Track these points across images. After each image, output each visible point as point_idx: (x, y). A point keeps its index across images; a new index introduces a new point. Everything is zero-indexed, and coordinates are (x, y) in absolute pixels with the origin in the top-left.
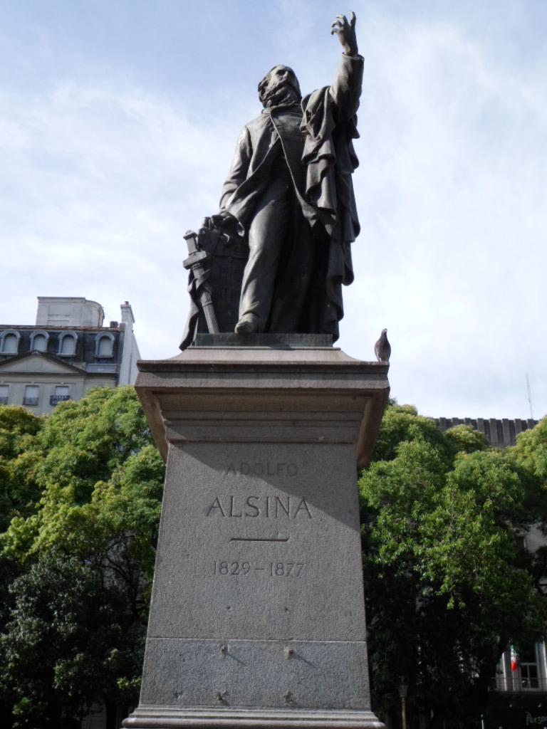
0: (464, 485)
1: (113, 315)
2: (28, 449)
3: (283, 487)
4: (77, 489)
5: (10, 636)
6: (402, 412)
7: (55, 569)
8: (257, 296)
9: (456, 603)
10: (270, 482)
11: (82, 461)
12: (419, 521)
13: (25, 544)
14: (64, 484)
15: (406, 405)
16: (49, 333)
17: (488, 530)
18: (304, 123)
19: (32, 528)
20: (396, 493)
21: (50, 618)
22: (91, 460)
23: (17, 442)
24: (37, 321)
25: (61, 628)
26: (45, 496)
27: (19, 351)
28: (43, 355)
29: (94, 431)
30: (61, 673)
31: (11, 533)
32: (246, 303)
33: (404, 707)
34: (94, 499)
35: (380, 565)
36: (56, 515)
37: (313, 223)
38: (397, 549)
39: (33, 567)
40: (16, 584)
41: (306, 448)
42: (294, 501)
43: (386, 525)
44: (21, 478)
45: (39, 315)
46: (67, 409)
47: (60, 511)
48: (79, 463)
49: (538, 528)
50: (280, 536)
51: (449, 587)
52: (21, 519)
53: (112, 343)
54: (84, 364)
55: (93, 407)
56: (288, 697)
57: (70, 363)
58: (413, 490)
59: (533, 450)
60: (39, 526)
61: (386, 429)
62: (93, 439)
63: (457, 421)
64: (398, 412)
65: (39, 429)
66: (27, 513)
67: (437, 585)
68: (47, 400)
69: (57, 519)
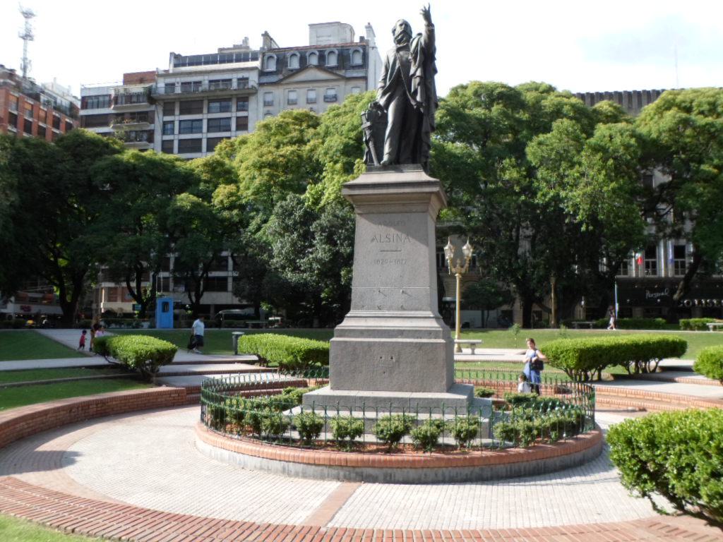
0: (597, 149)
1: (360, 32)
2: (312, 138)
3: (399, 230)
4: (344, 164)
5: (314, 255)
6: (560, 96)
7: (335, 216)
8: (391, 145)
9: (587, 228)
10: (395, 228)
11: (346, 145)
12: (564, 175)
13: (317, 201)
14: (336, 162)
15: (565, 91)
16: (318, 51)
17: (609, 178)
18: (410, 57)
19: (320, 191)
20: (550, 156)
21: (335, 244)
22: (352, 144)
23: (305, 134)
24: (310, 42)
25: (342, 250)
26: (326, 170)
27: (300, 66)
28: (317, 67)
29: (352, 125)
30: (345, 276)
31: (307, 194)
32: (387, 149)
33: (553, 291)
34: (355, 171)
35: (538, 204)
36: (333, 182)
37: (415, 107)
38: (549, 193)
39: (323, 215)
40: (314, 226)
41: (409, 214)
42: (404, 236)
43: (542, 178)
44: (310, 158)
45: (311, 38)
46: (334, 110)
47: (335, 180)
48: (344, 147)
49: (659, 171)
50: (399, 249)
51: (583, 217)
52: (313, 186)
53: (361, 54)
54: (344, 71)
55: (350, 108)
56: (402, 306)
57: (334, 72)
58: (561, 155)
59: (652, 119)
60: (324, 190)
61: (548, 110)
62: (352, 130)
63: (600, 96)
64: (557, 96)
65: (318, 124)
66: (316, 181)
67: (575, 214)
68: (321, 99)
69: (334, 185)
